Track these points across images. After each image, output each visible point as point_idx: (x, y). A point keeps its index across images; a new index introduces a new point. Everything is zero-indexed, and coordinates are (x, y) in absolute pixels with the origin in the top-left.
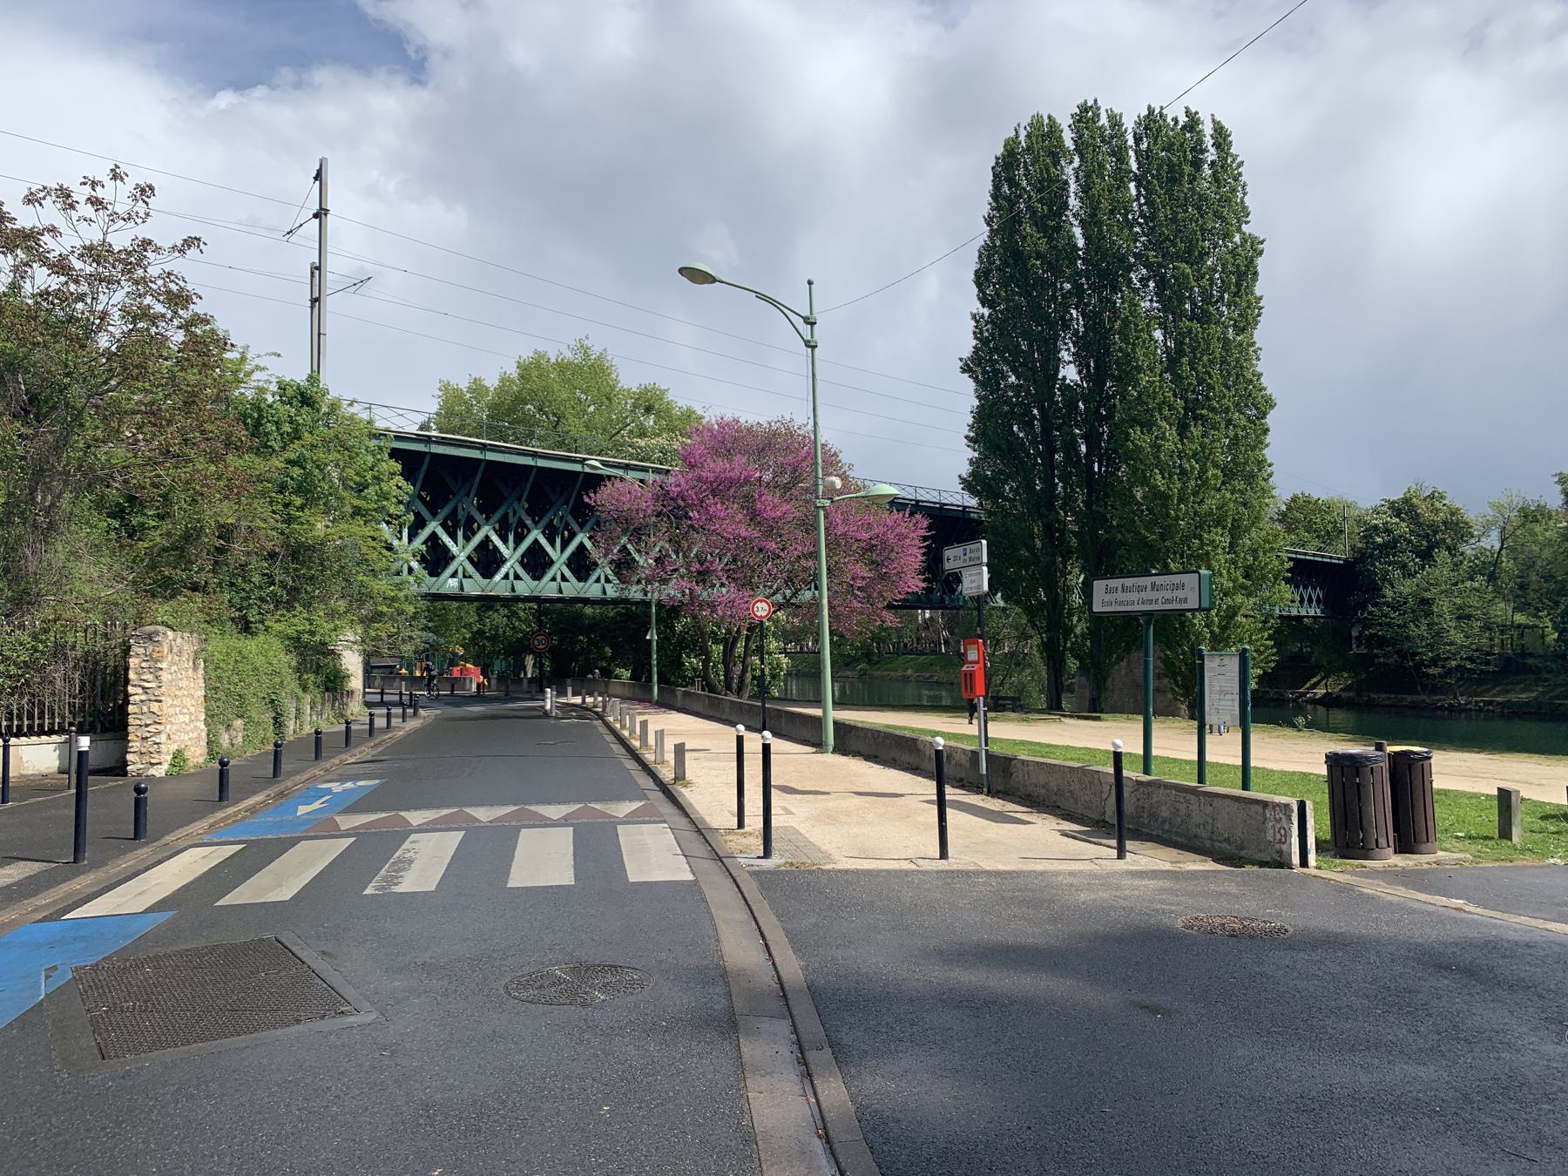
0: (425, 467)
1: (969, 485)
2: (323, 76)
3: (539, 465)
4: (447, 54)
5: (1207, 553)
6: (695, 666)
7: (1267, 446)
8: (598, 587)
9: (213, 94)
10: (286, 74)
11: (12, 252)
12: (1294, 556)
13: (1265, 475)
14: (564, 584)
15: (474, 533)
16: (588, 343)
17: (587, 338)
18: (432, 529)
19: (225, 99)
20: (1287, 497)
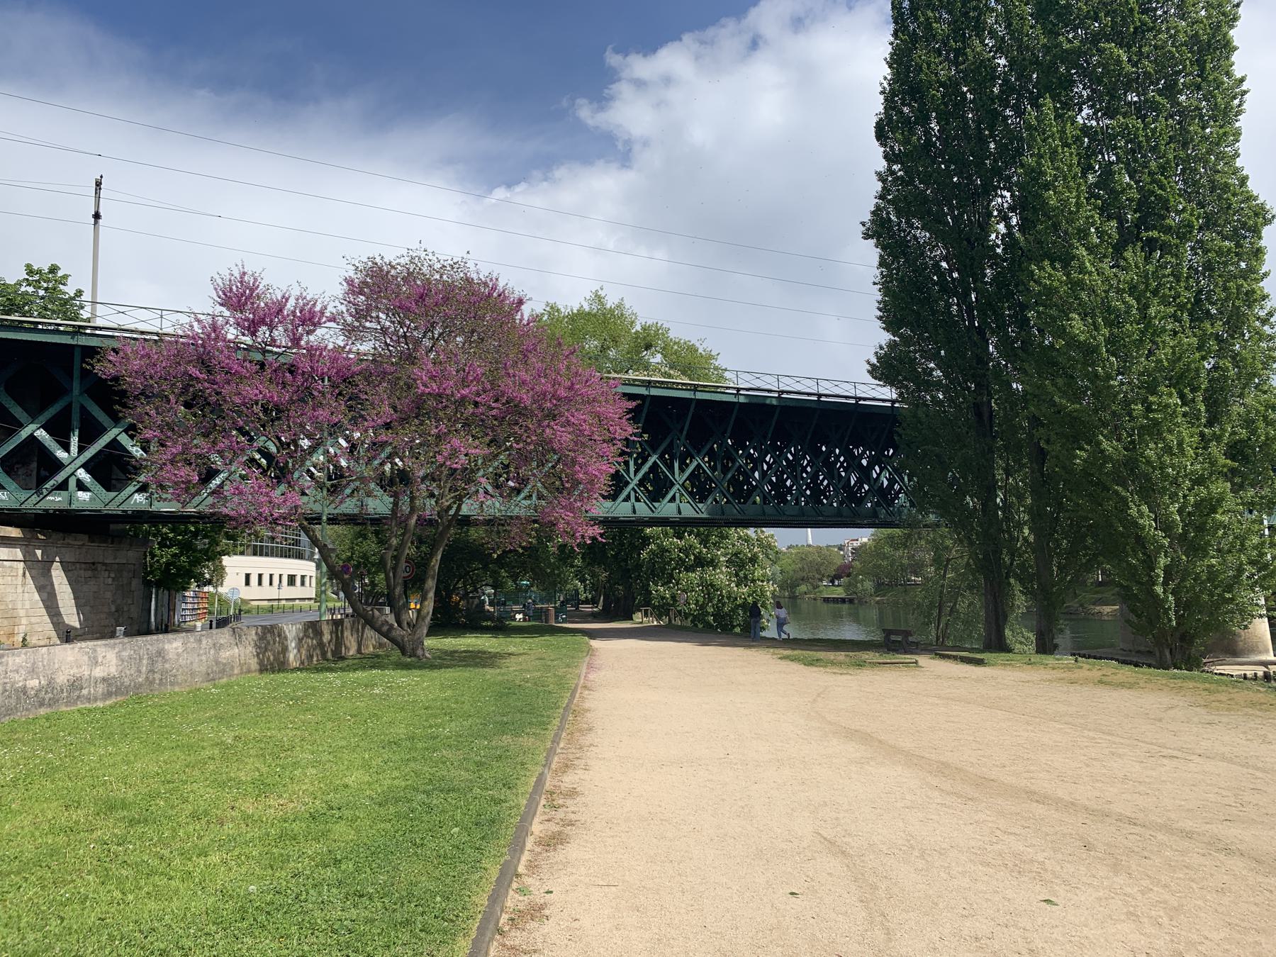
0: (692, 410)
1: (885, 369)
2: (559, 173)
3: (652, 394)
4: (646, 143)
5: (1156, 423)
6: (662, 594)
7: (1266, 275)
8: (628, 505)
9: (490, 191)
10: (537, 174)
11: (1110, 327)
12: (643, 391)
13: (1262, 314)
14: (637, 505)
15: (687, 465)
16: (602, 293)
17: (602, 289)
18: (113, 436)
19: (500, 193)
20: (339, 290)
